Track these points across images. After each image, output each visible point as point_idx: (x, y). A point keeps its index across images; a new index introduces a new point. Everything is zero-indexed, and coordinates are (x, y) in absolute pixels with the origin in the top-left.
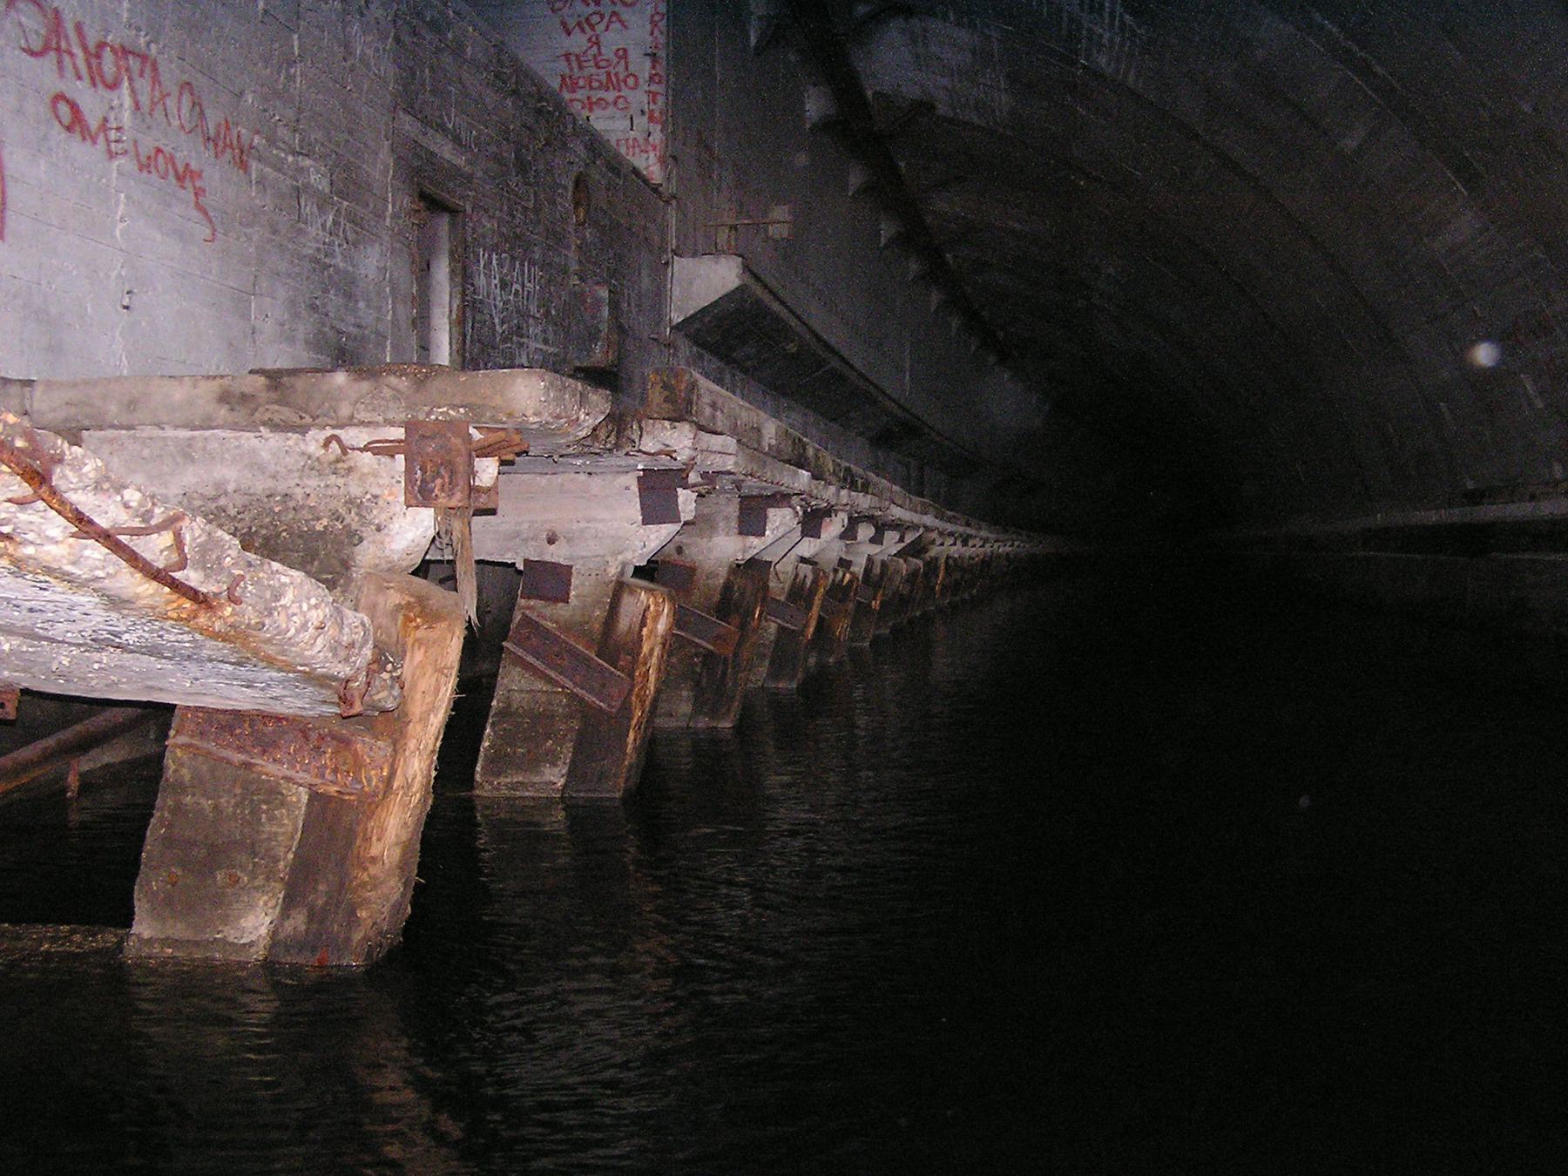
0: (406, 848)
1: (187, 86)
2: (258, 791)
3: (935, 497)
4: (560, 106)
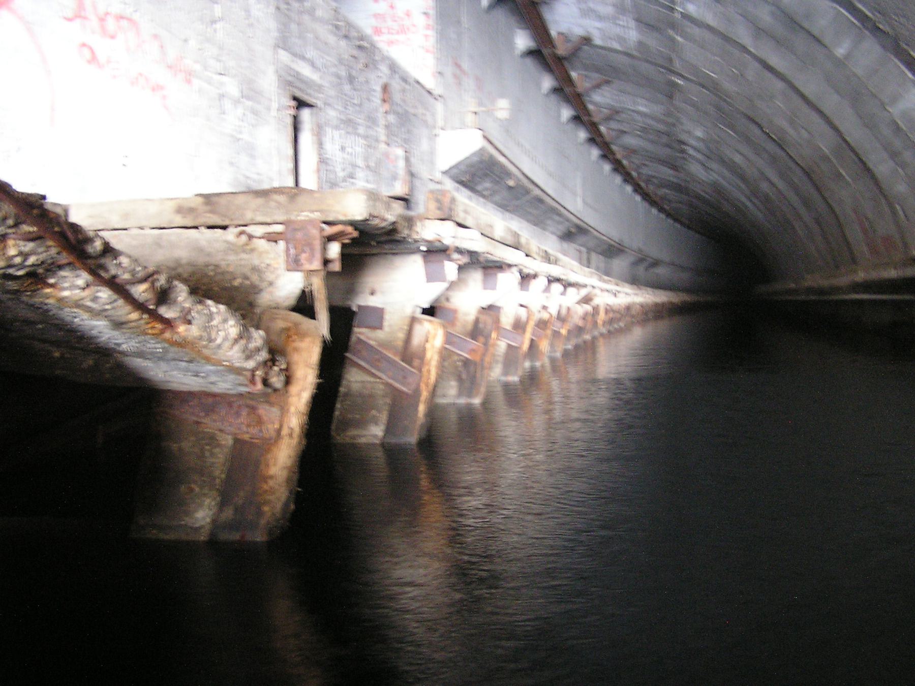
0: (290, 469)
1: (156, 36)
2: (203, 439)
3: (598, 269)
4: (373, 45)
